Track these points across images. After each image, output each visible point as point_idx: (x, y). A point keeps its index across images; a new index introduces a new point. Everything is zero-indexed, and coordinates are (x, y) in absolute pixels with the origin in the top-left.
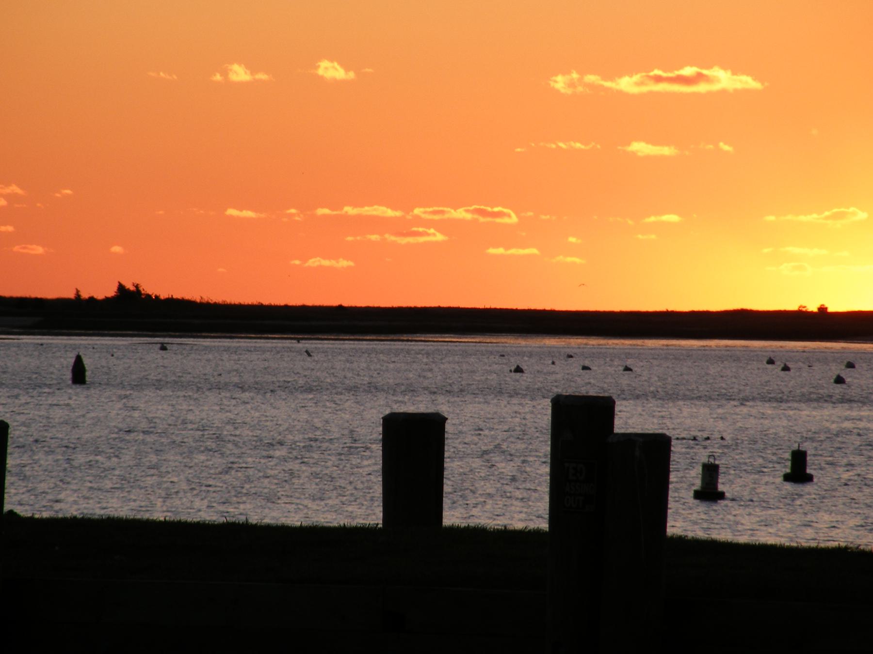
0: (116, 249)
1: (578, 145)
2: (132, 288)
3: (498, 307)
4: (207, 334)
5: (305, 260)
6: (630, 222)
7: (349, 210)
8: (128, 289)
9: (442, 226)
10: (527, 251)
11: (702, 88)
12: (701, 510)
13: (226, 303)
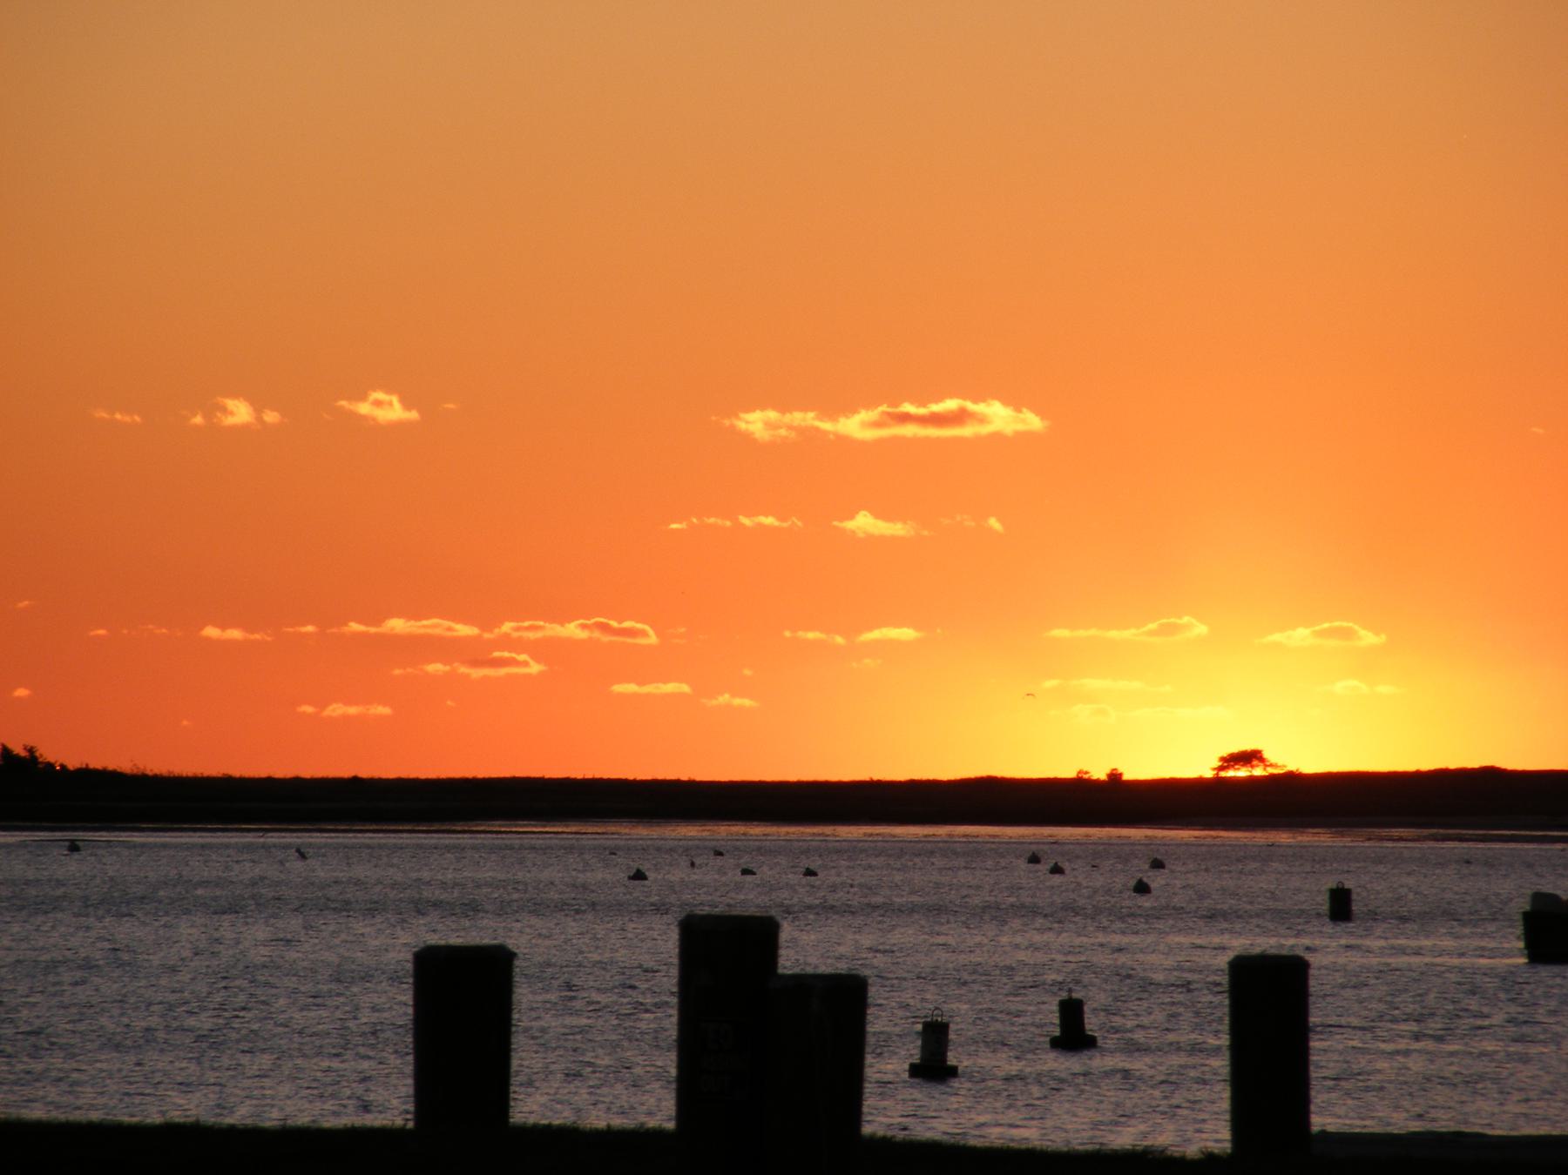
0: (21, 692)
1: (769, 521)
2: (23, 754)
3: (605, 777)
4: (68, 825)
5: (323, 705)
6: (839, 640)
7: (397, 625)
8: (17, 754)
9: (540, 649)
10: (670, 687)
11: (967, 431)
12: (921, 1094)
13: (172, 775)
